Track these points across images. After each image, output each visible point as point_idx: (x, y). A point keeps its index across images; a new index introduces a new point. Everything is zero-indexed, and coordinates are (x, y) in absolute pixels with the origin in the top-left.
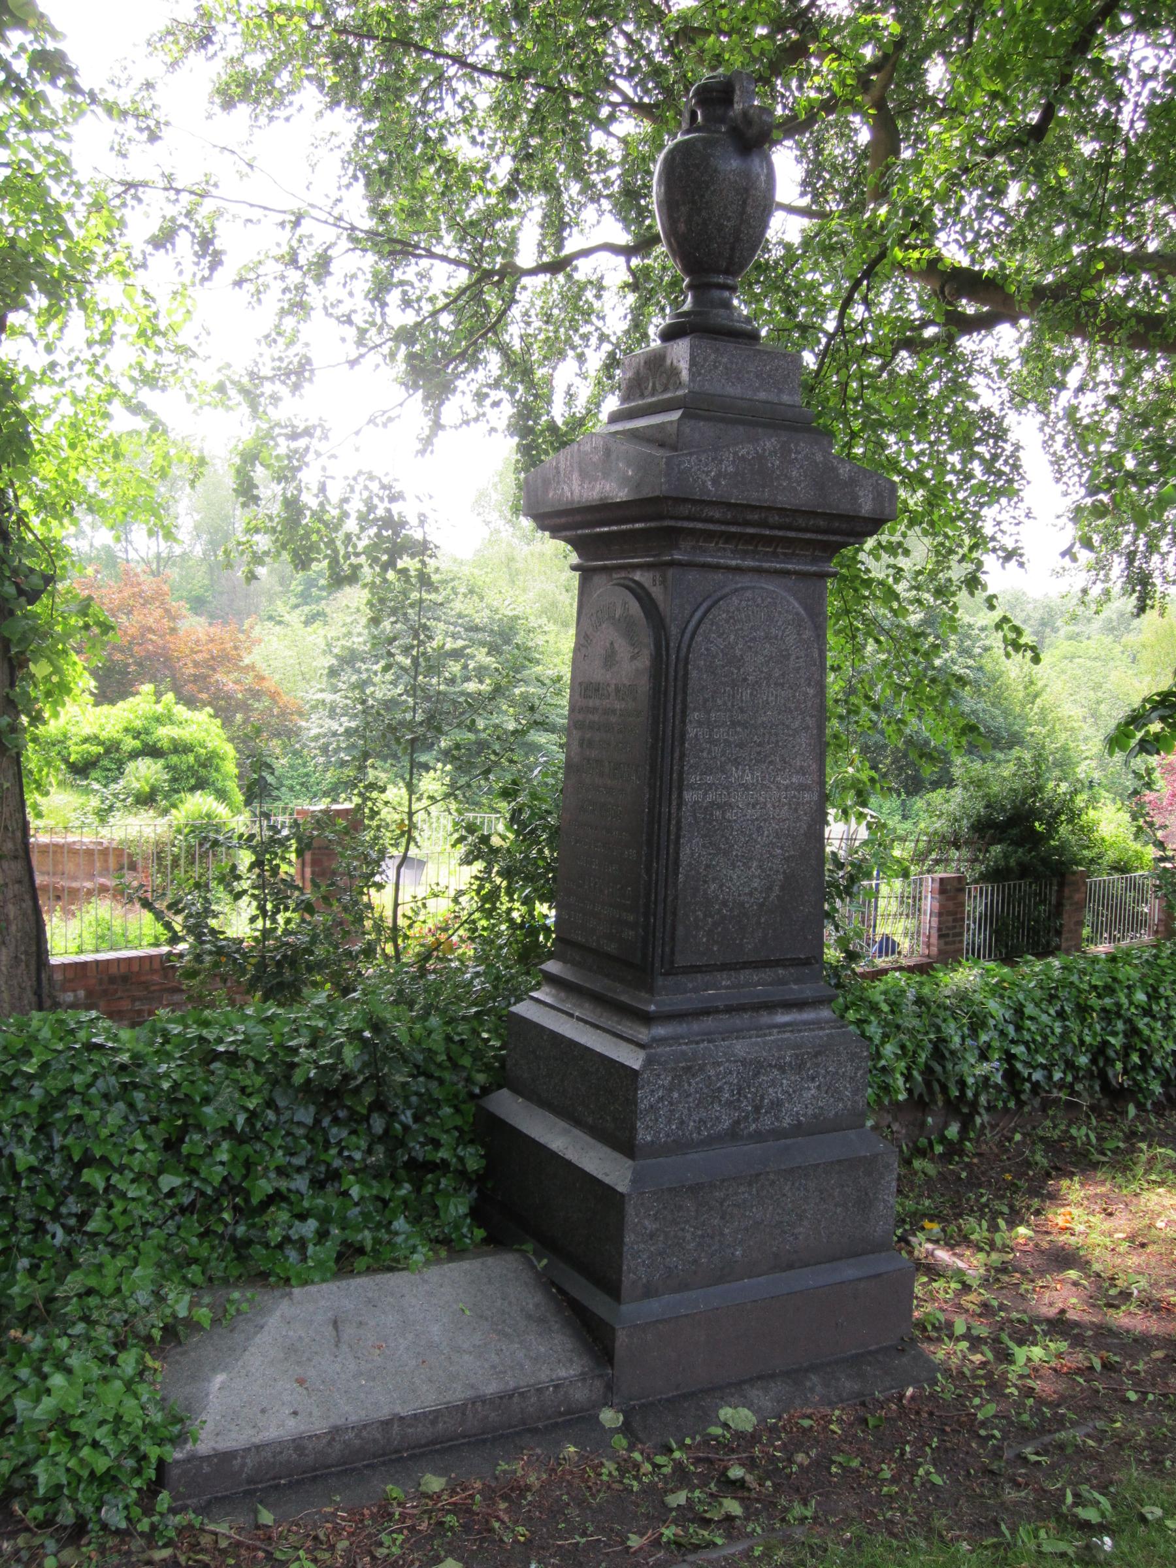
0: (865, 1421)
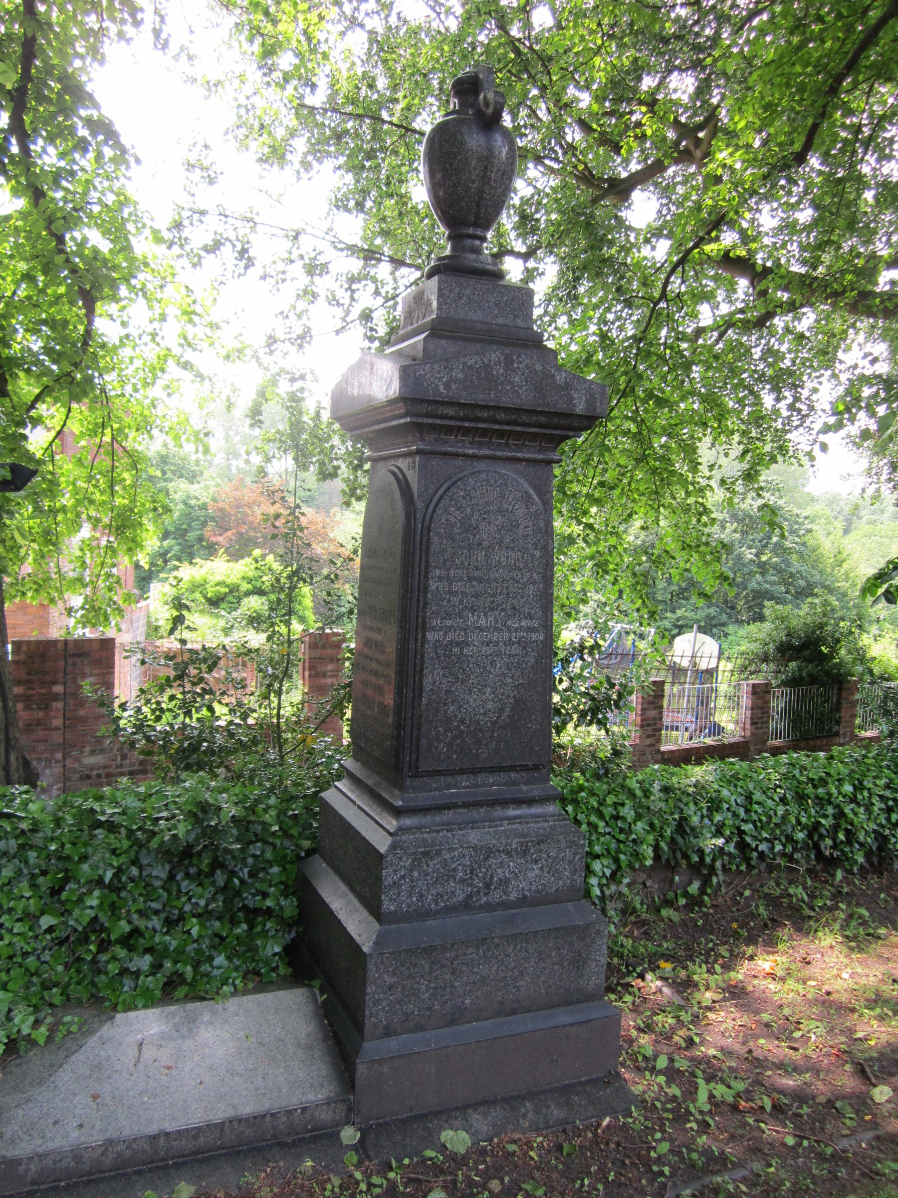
0: (560, 1148)
